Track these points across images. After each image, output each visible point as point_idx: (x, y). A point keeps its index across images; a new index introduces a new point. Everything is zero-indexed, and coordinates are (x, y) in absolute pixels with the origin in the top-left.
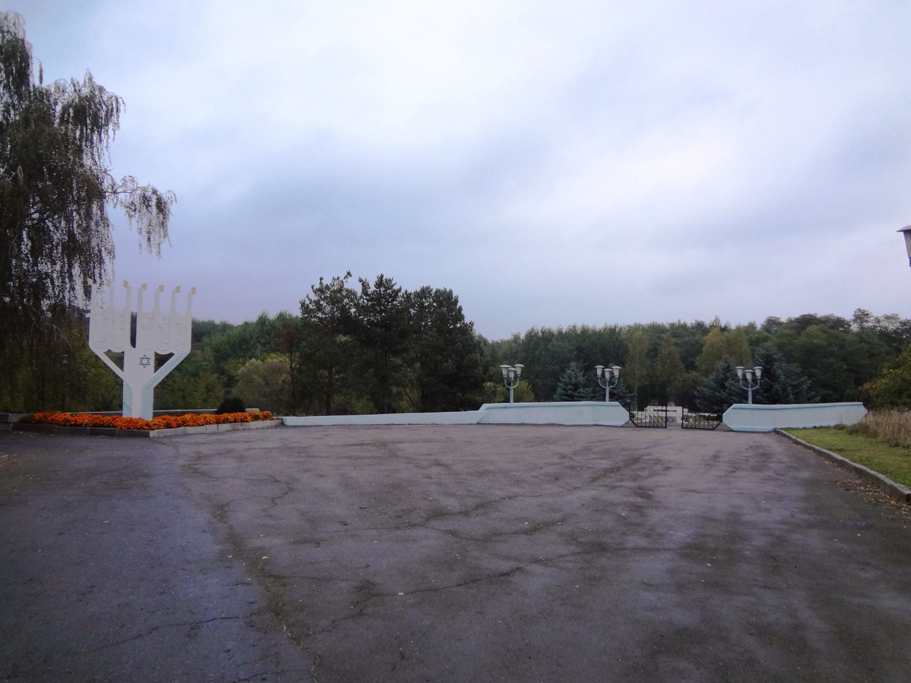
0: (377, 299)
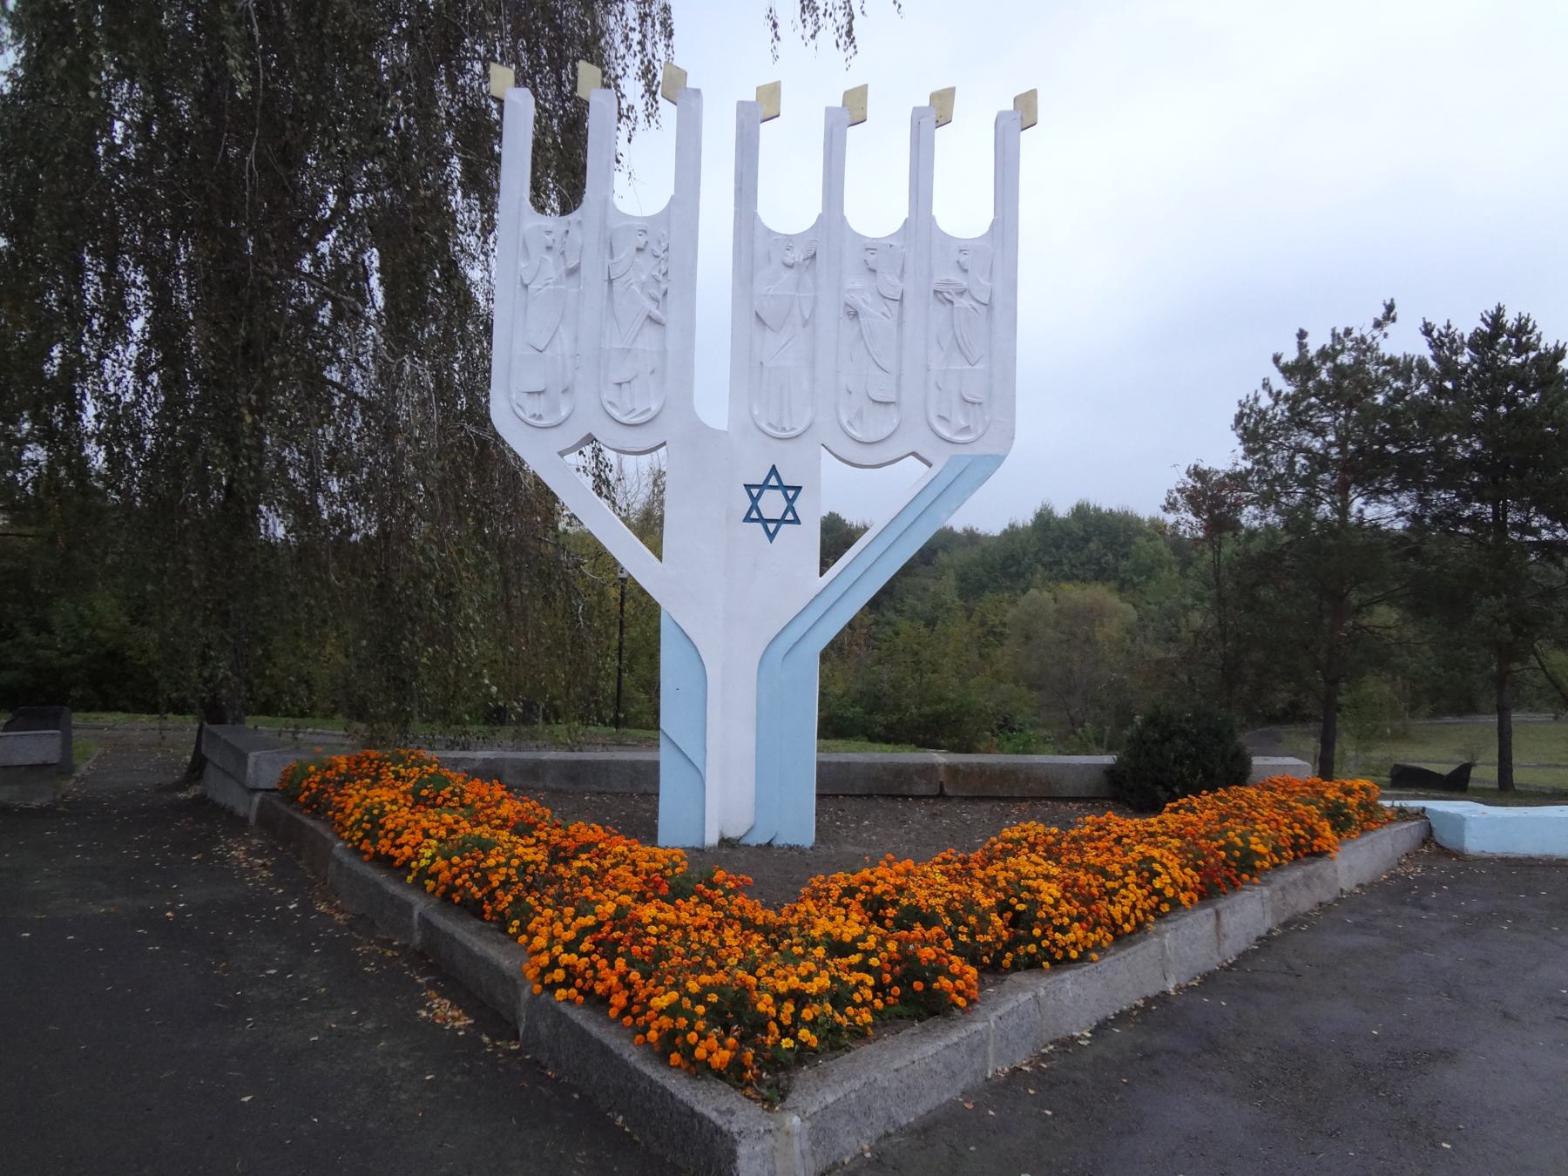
0: (1491, 378)
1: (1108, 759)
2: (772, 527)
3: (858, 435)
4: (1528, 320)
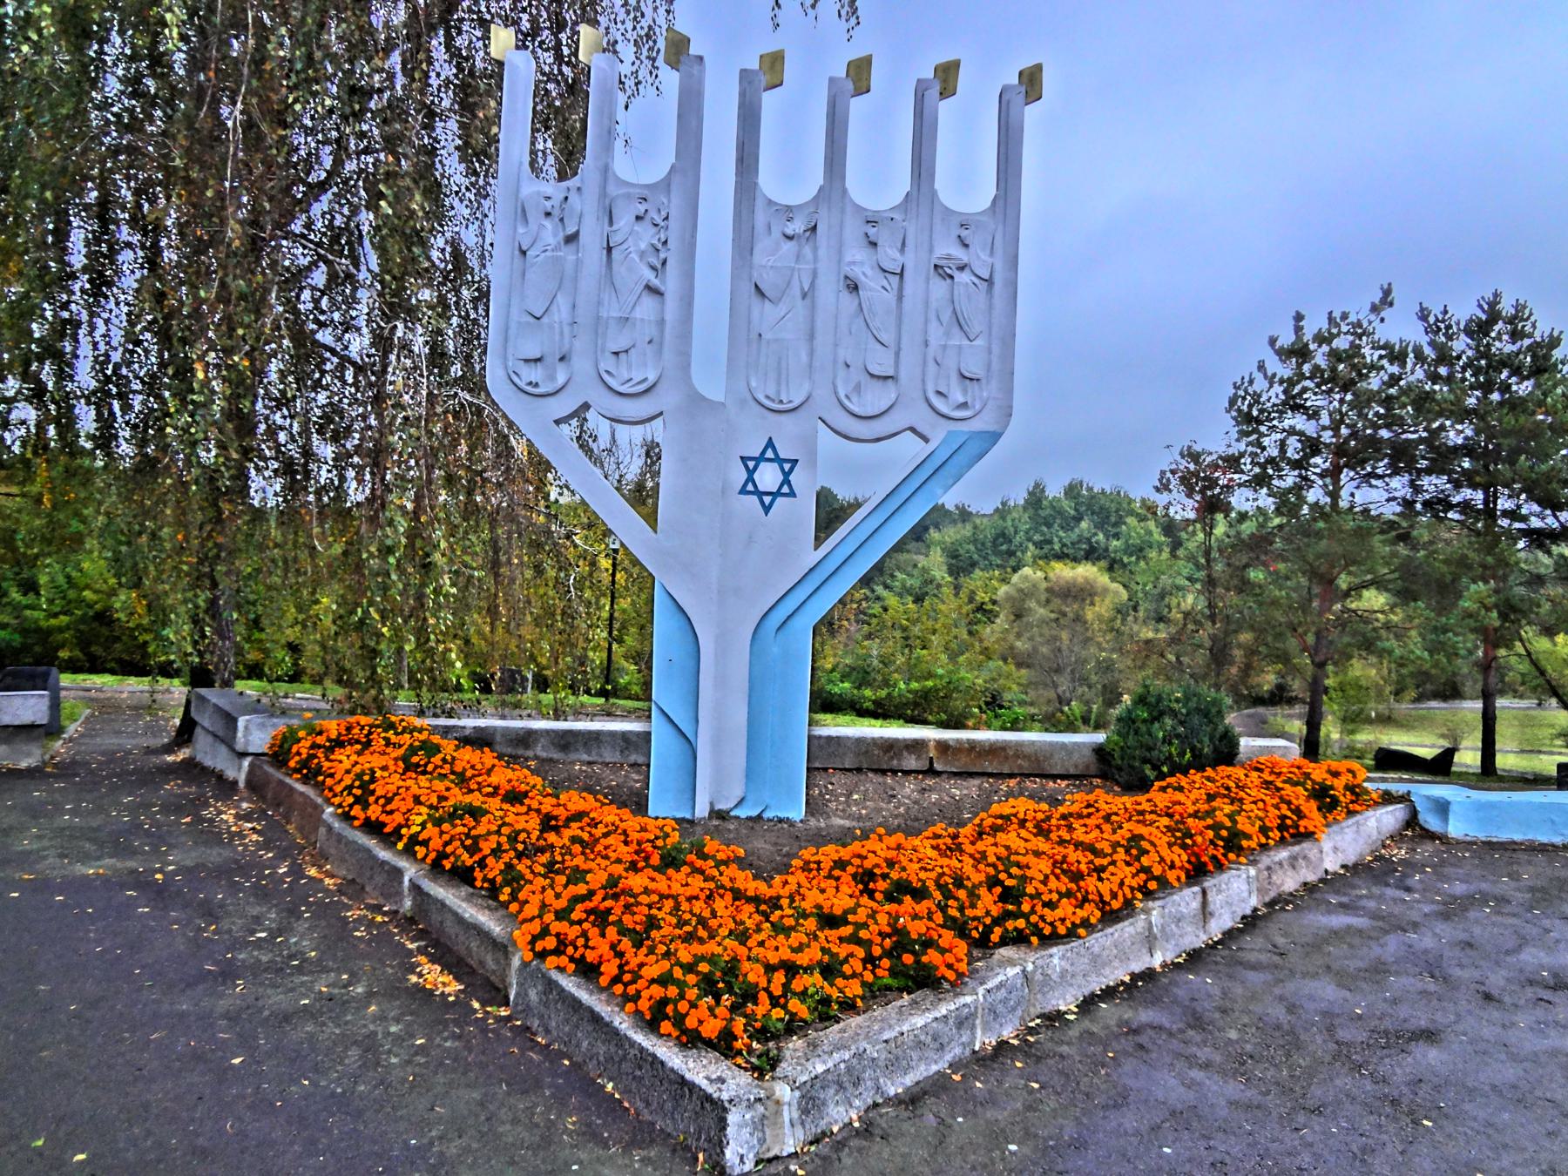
1: (1100, 737)
2: (767, 499)
3: (856, 410)
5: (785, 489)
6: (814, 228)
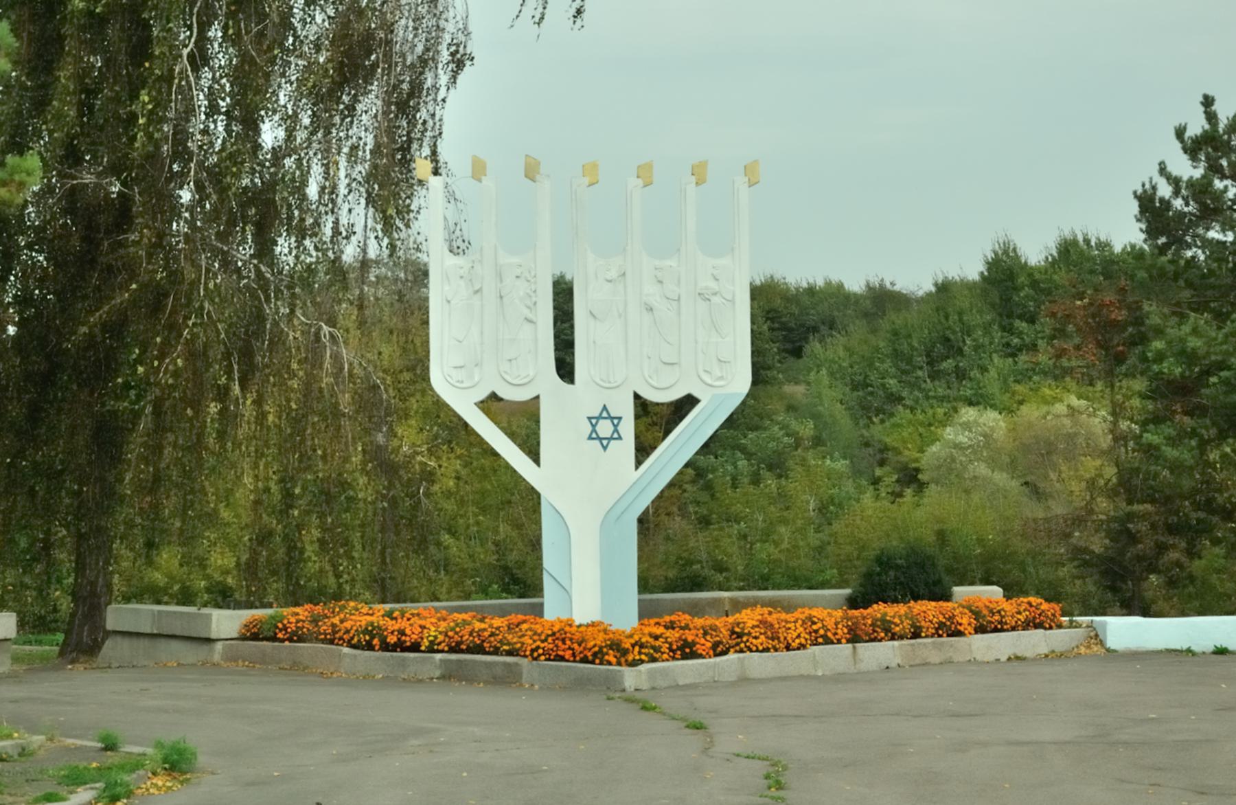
1: (848, 591)
2: (605, 442)
3: (655, 384)
4: (192, 772)
5: (616, 435)
6: (624, 274)
